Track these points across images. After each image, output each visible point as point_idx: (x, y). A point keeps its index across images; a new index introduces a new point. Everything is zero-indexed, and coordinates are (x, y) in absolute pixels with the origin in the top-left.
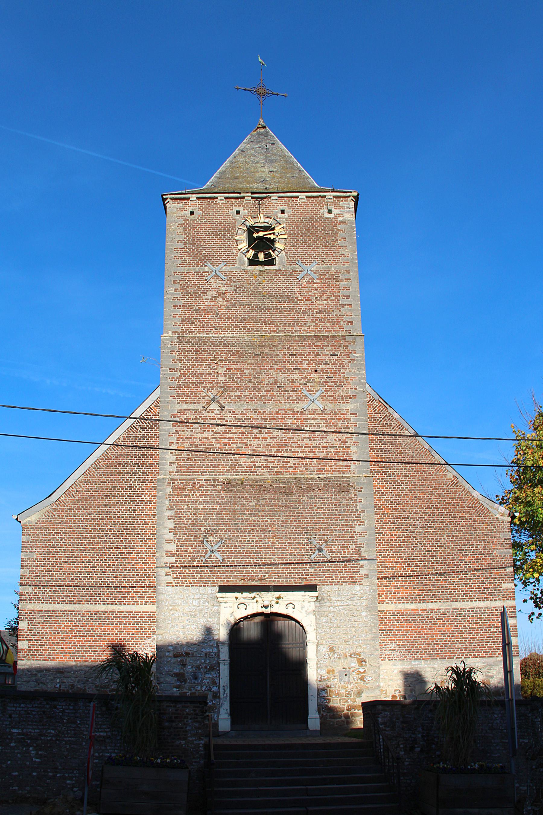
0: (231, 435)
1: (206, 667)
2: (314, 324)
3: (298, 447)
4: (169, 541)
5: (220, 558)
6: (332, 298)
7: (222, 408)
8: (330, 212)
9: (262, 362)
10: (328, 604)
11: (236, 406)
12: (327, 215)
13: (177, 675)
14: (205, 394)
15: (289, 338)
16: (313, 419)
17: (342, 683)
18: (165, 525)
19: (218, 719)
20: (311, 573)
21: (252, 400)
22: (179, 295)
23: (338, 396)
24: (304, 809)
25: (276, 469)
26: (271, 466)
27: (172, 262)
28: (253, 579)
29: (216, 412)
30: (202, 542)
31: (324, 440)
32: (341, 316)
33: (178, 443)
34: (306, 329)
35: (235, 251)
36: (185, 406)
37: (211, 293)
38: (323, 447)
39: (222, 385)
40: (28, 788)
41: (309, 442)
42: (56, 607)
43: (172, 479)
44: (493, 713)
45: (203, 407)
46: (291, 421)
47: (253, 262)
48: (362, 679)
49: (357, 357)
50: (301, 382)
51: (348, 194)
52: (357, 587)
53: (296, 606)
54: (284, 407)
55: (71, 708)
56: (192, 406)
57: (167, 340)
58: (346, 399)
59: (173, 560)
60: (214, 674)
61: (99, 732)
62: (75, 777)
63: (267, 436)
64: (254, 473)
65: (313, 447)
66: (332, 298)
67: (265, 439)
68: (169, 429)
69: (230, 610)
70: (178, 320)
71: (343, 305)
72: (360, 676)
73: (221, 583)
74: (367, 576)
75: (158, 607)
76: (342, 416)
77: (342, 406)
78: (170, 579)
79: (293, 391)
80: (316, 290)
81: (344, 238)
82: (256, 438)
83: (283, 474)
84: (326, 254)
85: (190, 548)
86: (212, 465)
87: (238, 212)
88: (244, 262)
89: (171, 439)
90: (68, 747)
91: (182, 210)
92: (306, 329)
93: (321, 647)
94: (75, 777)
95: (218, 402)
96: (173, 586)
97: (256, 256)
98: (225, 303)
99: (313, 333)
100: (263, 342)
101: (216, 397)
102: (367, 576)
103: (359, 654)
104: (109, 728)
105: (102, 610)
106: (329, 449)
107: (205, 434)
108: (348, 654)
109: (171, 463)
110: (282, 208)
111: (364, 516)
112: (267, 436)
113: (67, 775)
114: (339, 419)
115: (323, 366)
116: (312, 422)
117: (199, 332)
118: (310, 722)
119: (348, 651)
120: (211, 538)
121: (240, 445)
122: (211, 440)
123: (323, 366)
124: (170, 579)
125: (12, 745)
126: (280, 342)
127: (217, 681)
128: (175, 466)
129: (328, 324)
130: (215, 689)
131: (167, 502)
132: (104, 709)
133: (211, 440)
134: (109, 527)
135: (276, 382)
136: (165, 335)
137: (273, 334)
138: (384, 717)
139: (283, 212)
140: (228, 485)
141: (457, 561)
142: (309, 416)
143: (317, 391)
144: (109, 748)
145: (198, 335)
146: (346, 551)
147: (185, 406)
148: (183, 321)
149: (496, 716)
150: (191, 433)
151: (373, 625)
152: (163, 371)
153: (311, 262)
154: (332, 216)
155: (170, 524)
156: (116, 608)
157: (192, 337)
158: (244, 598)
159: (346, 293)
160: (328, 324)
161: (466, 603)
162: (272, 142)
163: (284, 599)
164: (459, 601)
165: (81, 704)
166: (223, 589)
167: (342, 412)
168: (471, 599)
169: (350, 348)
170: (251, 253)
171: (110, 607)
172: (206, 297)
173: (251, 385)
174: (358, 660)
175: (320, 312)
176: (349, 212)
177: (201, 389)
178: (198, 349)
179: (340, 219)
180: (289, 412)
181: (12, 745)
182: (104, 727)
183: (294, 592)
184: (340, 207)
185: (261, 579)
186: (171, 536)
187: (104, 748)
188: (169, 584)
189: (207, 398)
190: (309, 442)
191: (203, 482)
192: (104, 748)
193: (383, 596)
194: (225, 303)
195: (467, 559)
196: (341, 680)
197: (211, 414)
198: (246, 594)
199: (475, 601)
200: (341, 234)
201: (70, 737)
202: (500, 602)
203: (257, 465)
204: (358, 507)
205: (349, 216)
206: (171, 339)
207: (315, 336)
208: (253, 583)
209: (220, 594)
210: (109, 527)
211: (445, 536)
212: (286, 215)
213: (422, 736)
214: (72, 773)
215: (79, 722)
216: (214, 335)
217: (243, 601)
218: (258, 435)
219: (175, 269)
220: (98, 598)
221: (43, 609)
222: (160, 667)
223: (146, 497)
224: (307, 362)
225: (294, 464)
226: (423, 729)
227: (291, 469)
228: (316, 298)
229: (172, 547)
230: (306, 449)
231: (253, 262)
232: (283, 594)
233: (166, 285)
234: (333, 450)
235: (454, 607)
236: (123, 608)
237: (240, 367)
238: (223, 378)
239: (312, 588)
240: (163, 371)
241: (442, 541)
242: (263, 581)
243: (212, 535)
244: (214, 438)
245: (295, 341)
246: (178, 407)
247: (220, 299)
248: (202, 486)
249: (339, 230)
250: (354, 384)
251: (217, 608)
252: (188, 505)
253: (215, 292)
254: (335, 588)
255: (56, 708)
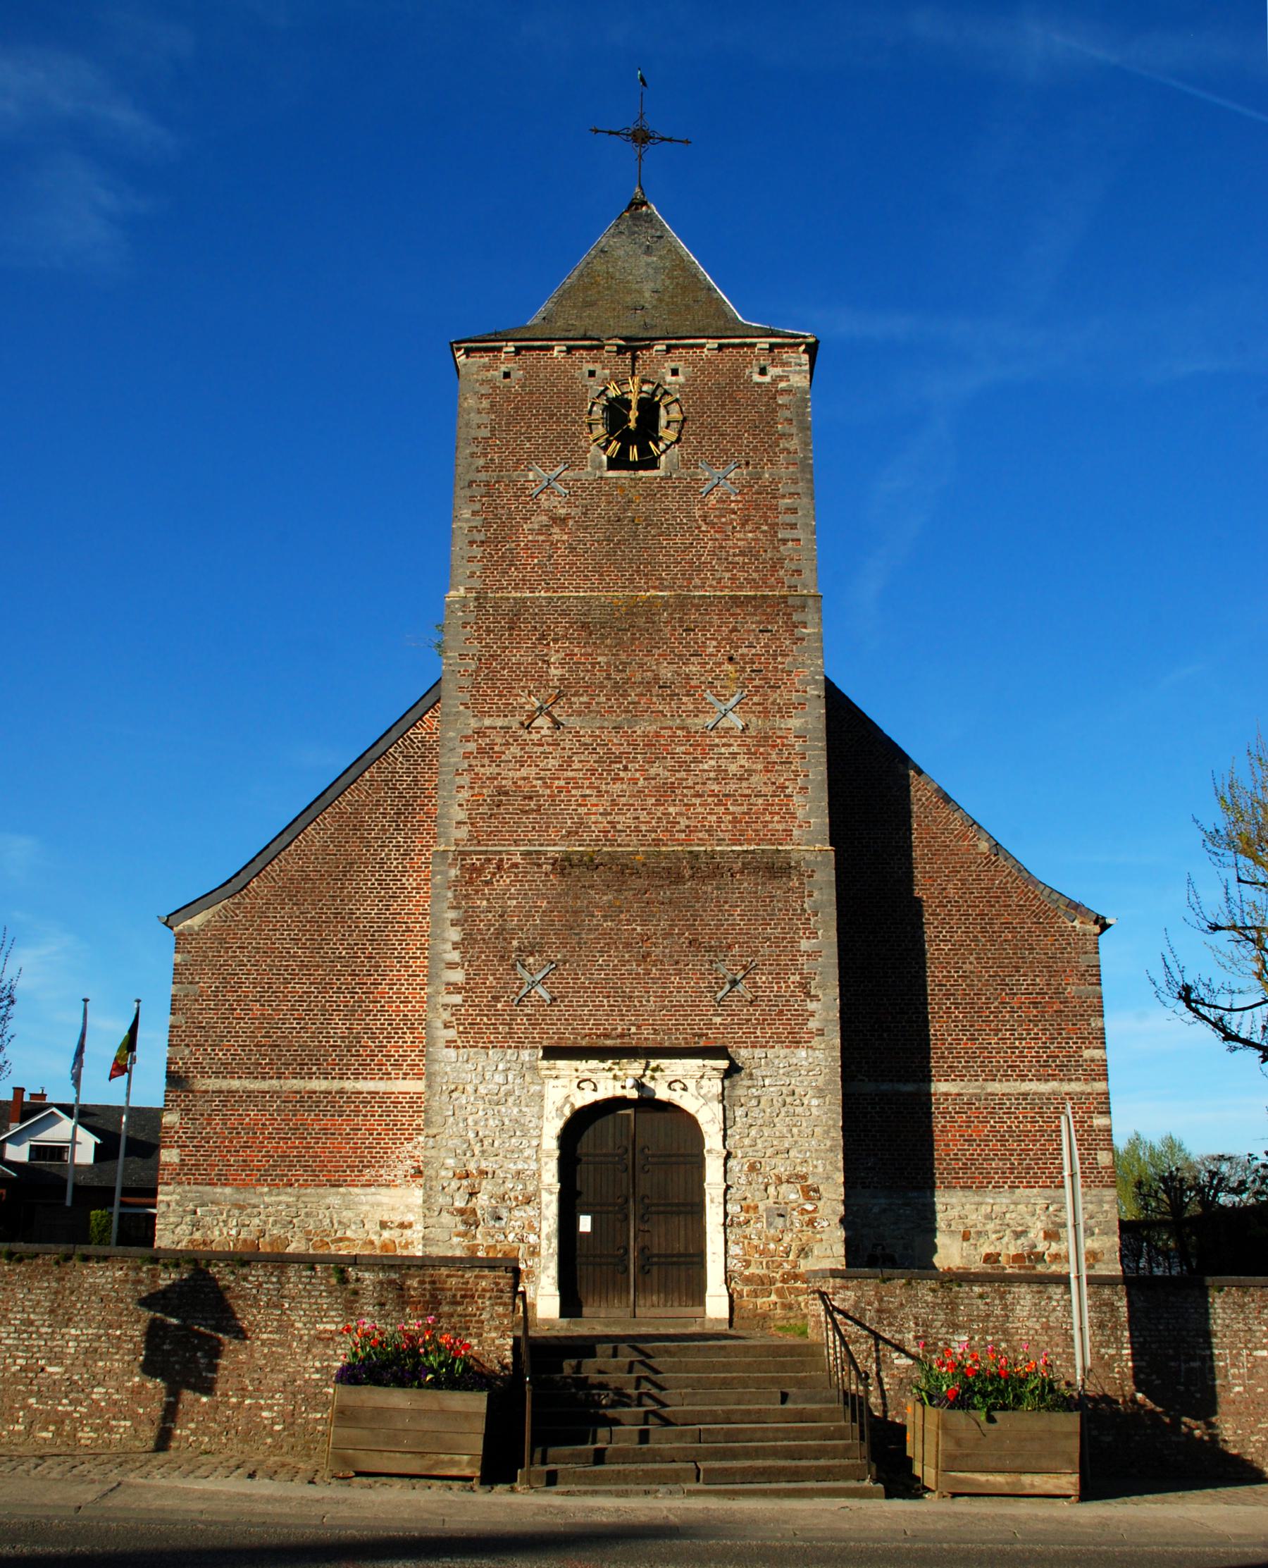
0: (570, 774)
1: (516, 1198)
2: (727, 575)
3: (695, 796)
4: (451, 966)
5: (547, 996)
6: (765, 528)
7: (557, 725)
8: (763, 372)
9: (632, 644)
10: (747, 1083)
11: (582, 721)
12: (757, 378)
13: (461, 1212)
14: (524, 700)
15: (683, 603)
16: (724, 745)
17: (772, 1231)
18: (446, 935)
19: (536, 1294)
20: (717, 1027)
21: (610, 711)
22: (477, 522)
23: (773, 703)
24: (692, 1465)
25: (653, 835)
26: (644, 829)
27: (467, 461)
28: (606, 1036)
29: (544, 732)
30: (513, 966)
31: (744, 784)
32: (781, 560)
33: (472, 788)
34: (714, 583)
35: (583, 443)
36: (487, 722)
37: (540, 518)
38: (741, 795)
39: (558, 684)
40: (192, 1425)
41: (716, 788)
42: (235, 1084)
43: (461, 853)
44: (1050, 1298)
45: (522, 724)
46: (683, 749)
47: (617, 463)
48: (811, 1222)
49: (809, 635)
50: (703, 678)
51: (798, 340)
52: (802, 1053)
53: (690, 1086)
54: (670, 723)
55: (274, 1280)
56: (499, 722)
57: (457, 602)
58: (784, 711)
59: (457, 999)
60: (530, 1211)
61: (322, 1322)
62: (279, 1405)
63: (637, 775)
64: (612, 842)
65: (725, 795)
66: (765, 528)
67: (634, 781)
68: (456, 763)
69: (562, 1093)
70: (476, 567)
71: (785, 541)
72: (806, 1218)
73: (545, 1043)
74: (821, 1033)
75: (429, 1086)
76: (779, 741)
77: (778, 722)
78: (451, 1034)
79: (688, 695)
80: (735, 513)
81: (790, 421)
82: (617, 779)
83: (666, 845)
84: (755, 449)
85: (491, 978)
86: (534, 828)
87: (592, 374)
88: (601, 462)
89: (460, 781)
90: (266, 1351)
91: (487, 368)
92: (714, 583)
93: (731, 1163)
94: (279, 1405)
95: (549, 714)
96: (458, 1047)
97: (624, 452)
98: (565, 537)
99: (726, 592)
100: (632, 609)
101: (545, 706)
102: (821, 1033)
103: (804, 1177)
104: (340, 1315)
105: (323, 1088)
106: (753, 800)
107: (524, 772)
108: (784, 1178)
109: (458, 823)
110: (673, 365)
111: (816, 921)
112: (637, 775)
113: (262, 1402)
114: (774, 746)
115: (745, 650)
116: (723, 750)
117: (516, 588)
118: (709, 1300)
119: (782, 1169)
120: (531, 960)
121: (588, 792)
122: (535, 782)
123: (745, 650)
124: (451, 1034)
125: (165, 1347)
126: (666, 605)
127: (536, 1225)
128: (465, 828)
129: (755, 575)
130: (532, 1239)
131: (450, 894)
132: (334, 1281)
133: (535, 782)
134: (340, 936)
135: (656, 678)
136: (452, 593)
137: (652, 593)
138: (844, 1300)
139: (675, 372)
140: (564, 865)
141: (996, 1004)
142: (717, 740)
143: (733, 696)
144: (339, 1352)
145: (514, 594)
146: (783, 985)
147: (487, 722)
148: (485, 568)
149: (1054, 1303)
150: (497, 770)
151: (831, 1122)
152: (448, 658)
153: (726, 463)
154: (767, 379)
155: (455, 934)
156: (349, 1085)
157: (502, 598)
158: (590, 1070)
159: (789, 518)
160: (755, 575)
161: (1012, 1083)
162: (658, 234)
163: (667, 1072)
164: (1000, 1081)
165: (291, 1272)
166: (553, 1053)
167: (779, 733)
168: (1023, 1078)
169: (795, 618)
170: (615, 446)
171: (336, 1085)
172: (530, 526)
173: (609, 684)
174: (802, 1187)
175: (742, 554)
176: (799, 372)
177: (515, 691)
178: (515, 617)
179: (782, 385)
180: (679, 732)
181: (165, 1347)
182: (333, 1313)
183: (684, 1061)
184: (784, 364)
185: (622, 1036)
186: (455, 956)
187: (331, 1352)
188: (449, 1044)
189: (527, 707)
190: (716, 788)
191: (518, 859)
192: (331, 1352)
193: (853, 1068)
194: (565, 537)
195: (1015, 1002)
196: (770, 1224)
197: (535, 737)
198: (593, 1064)
199: (1031, 1080)
200: (783, 414)
201: (271, 1332)
202: (1079, 1083)
203: (619, 827)
204: (806, 906)
205: (799, 380)
206: (464, 602)
207: (731, 597)
208: (609, 1043)
209: (545, 1062)
210: (340, 936)
211: (972, 959)
212: (681, 379)
213: (916, 1338)
214: (273, 1397)
215: (287, 1306)
216: (543, 594)
217: (587, 1075)
218: (622, 774)
219: (472, 476)
220: (314, 1068)
221: (210, 1088)
222: (429, 1196)
223: (410, 883)
224: (714, 643)
225: (687, 827)
226: (917, 1324)
227: (683, 836)
228: (734, 528)
229: (458, 976)
230: (710, 800)
231: (617, 463)
232: (664, 1063)
233: (458, 502)
234: (760, 801)
235: (989, 1090)
236: (362, 1085)
237: (590, 651)
238: (558, 672)
239: (718, 1052)
240: (448, 658)
241: (967, 967)
242: (626, 1040)
243: (532, 954)
244: (540, 779)
245: (693, 605)
246: (474, 723)
247: (555, 530)
248: (516, 865)
249: (780, 405)
250: (802, 682)
251: (538, 1088)
252: (488, 900)
253: (544, 518)
254: (759, 1053)
255: (245, 1279)
